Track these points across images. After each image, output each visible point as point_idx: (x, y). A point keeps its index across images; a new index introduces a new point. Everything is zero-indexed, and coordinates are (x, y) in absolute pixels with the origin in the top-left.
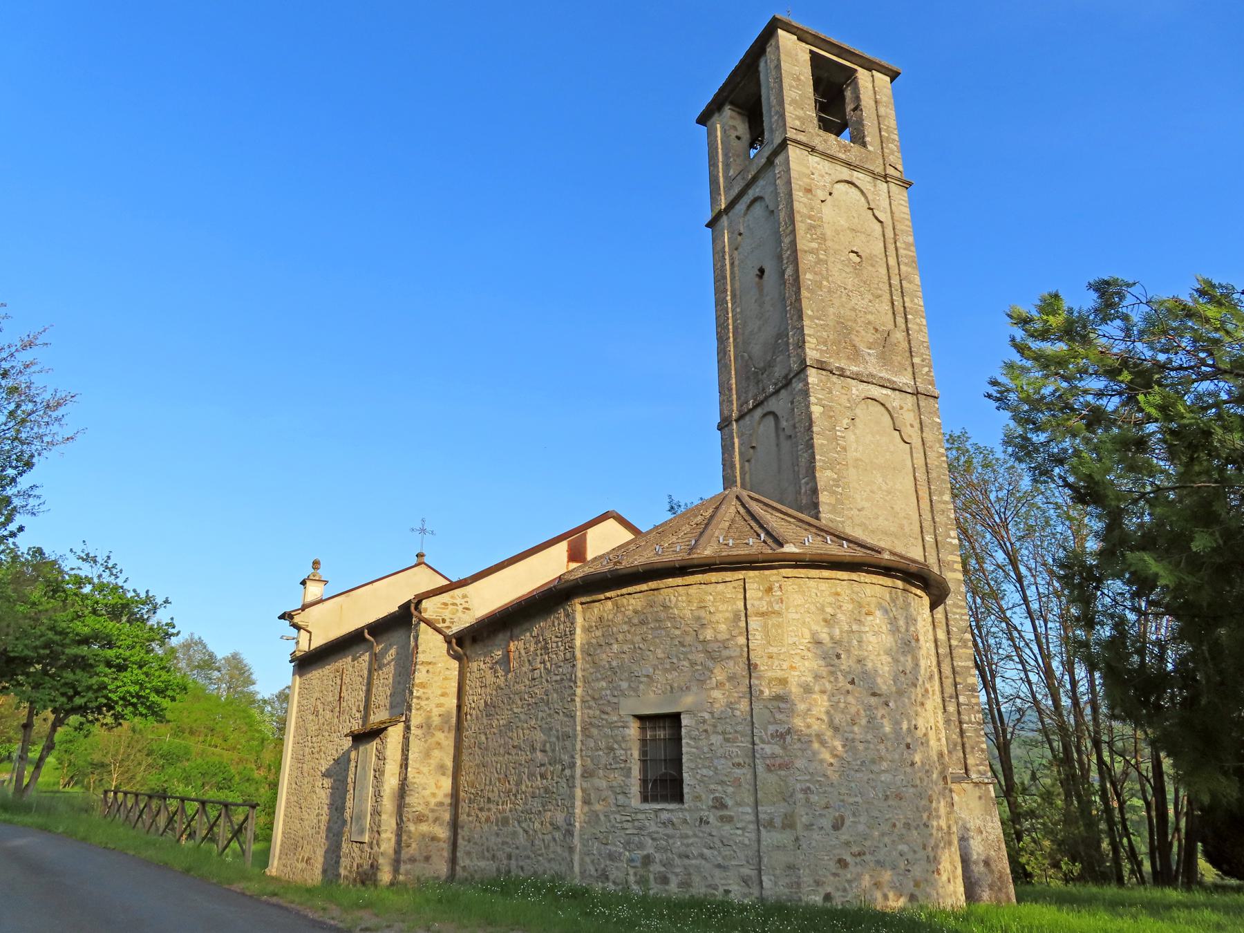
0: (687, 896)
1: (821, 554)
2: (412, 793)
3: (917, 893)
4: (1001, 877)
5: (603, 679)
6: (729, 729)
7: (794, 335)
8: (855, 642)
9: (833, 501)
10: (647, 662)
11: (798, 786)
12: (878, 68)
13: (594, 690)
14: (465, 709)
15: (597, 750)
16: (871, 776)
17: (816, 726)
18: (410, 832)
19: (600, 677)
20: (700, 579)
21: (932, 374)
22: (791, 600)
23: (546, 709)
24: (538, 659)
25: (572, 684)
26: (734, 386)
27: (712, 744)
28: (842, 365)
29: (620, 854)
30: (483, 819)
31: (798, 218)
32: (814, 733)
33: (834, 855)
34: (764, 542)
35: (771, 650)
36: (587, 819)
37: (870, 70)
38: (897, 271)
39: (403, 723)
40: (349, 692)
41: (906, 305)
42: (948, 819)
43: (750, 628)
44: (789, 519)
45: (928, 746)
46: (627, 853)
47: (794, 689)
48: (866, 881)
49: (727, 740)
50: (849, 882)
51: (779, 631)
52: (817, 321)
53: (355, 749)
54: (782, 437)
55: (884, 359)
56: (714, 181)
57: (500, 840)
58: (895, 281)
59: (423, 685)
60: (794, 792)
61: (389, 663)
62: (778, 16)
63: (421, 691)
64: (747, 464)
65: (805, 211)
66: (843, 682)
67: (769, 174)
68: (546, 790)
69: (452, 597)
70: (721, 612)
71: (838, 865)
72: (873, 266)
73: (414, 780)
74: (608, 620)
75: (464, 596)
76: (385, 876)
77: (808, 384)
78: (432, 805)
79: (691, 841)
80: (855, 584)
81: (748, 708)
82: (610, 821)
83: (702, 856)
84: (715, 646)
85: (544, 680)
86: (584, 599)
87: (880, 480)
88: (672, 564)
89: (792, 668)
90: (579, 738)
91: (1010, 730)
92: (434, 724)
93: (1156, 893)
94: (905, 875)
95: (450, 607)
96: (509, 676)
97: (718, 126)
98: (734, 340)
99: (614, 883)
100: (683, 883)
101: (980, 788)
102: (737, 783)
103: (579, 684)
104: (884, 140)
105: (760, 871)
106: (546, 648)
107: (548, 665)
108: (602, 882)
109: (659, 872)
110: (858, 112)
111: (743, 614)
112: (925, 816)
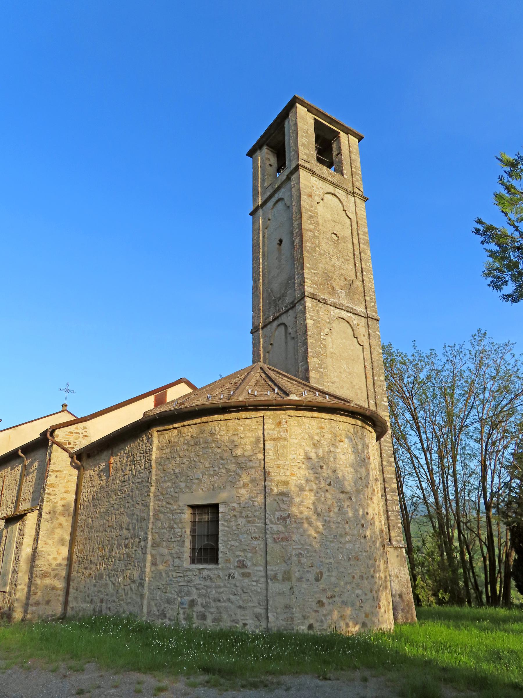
0: (218, 628)
1: (313, 402)
2: (40, 558)
3: (367, 622)
4: (408, 604)
5: (169, 481)
6: (250, 514)
7: (298, 278)
8: (332, 459)
9: (318, 377)
10: (198, 470)
11: (294, 552)
12: (352, 133)
13: (163, 488)
14: (80, 501)
15: (163, 529)
16: (341, 545)
17: (306, 513)
18: (37, 584)
19: (167, 479)
20: (235, 416)
21: (376, 307)
22: (293, 430)
23: (131, 501)
24: (128, 468)
25: (148, 484)
26: (261, 308)
27: (239, 525)
28: (326, 298)
29: (175, 599)
30: (87, 575)
31: (303, 210)
32: (304, 517)
33: (316, 598)
34: (277, 393)
35: (280, 462)
36: (153, 575)
37: (347, 134)
38: (358, 247)
39: (37, 511)
40: (7, 490)
41: (363, 266)
42: (385, 572)
43: (266, 448)
44: (293, 382)
45: (374, 526)
46: (179, 599)
47: (292, 487)
48: (336, 615)
49: (249, 522)
50: (325, 616)
51: (285, 450)
52: (312, 271)
53: (6, 528)
54: (289, 338)
55: (350, 295)
56: (255, 189)
57: (96, 589)
58: (357, 252)
59: (52, 486)
60: (291, 556)
61: (33, 471)
62: (297, 96)
63: (51, 489)
64: (267, 354)
65: (307, 207)
66: (323, 485)
67: (288, 185)
68: (128, 555)
69: (76, 428)
70: (248, 437)
71: (318, 605)
72: (345, 243)
73: (42, 549)
74: (174, 442)
75: (85, 428)
76: (18, 615)
77: (305, 306)
78: (54, 566)
79: (222, 590)
80: (333, 422)
81: (263, 501)
82: (169, 577)
83: (229, 600)
84: (243, 460)
85: (131, 482)
86: (159, 429)
87: (345, 366)
88: (217, 405)
89: (292, 474)
90: (151, 520)
91: (410, 515)
92: (59, 511)
93: (490, 610)
94: (359, 610)
95: (75, 435)
96: (109, 479)
97: (259, 158)
98: (263, 281)
99: (170, 619)
100: (215, 619)
101: (397, 550)
102: (254, 551)
103: (153, 484)
104: (354, 173)
105: (267, 609)
106: (133, 461)
107: (134, 471)
108: (162, 619)
109: (200, 612)
110: (340, 156)
111: (262, 439)
112: (372, 571)
